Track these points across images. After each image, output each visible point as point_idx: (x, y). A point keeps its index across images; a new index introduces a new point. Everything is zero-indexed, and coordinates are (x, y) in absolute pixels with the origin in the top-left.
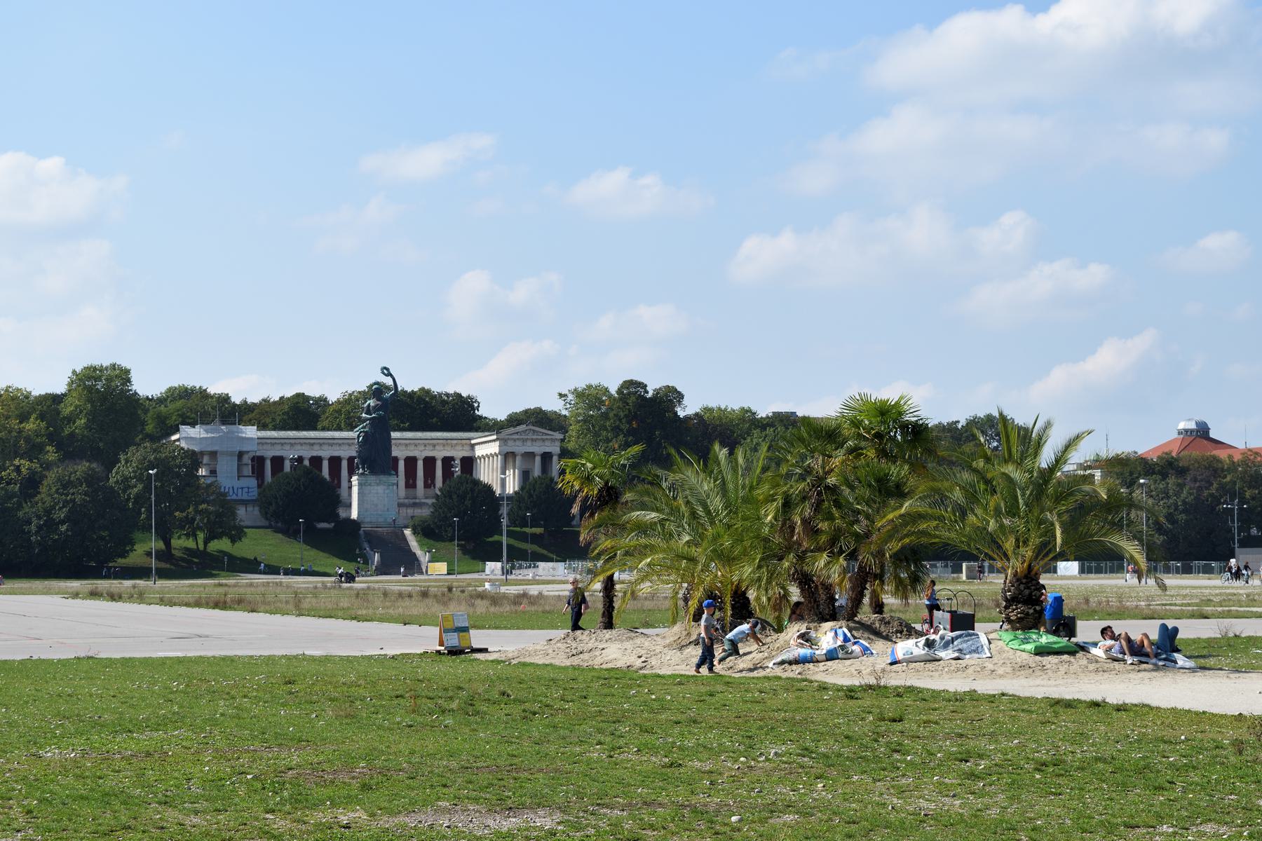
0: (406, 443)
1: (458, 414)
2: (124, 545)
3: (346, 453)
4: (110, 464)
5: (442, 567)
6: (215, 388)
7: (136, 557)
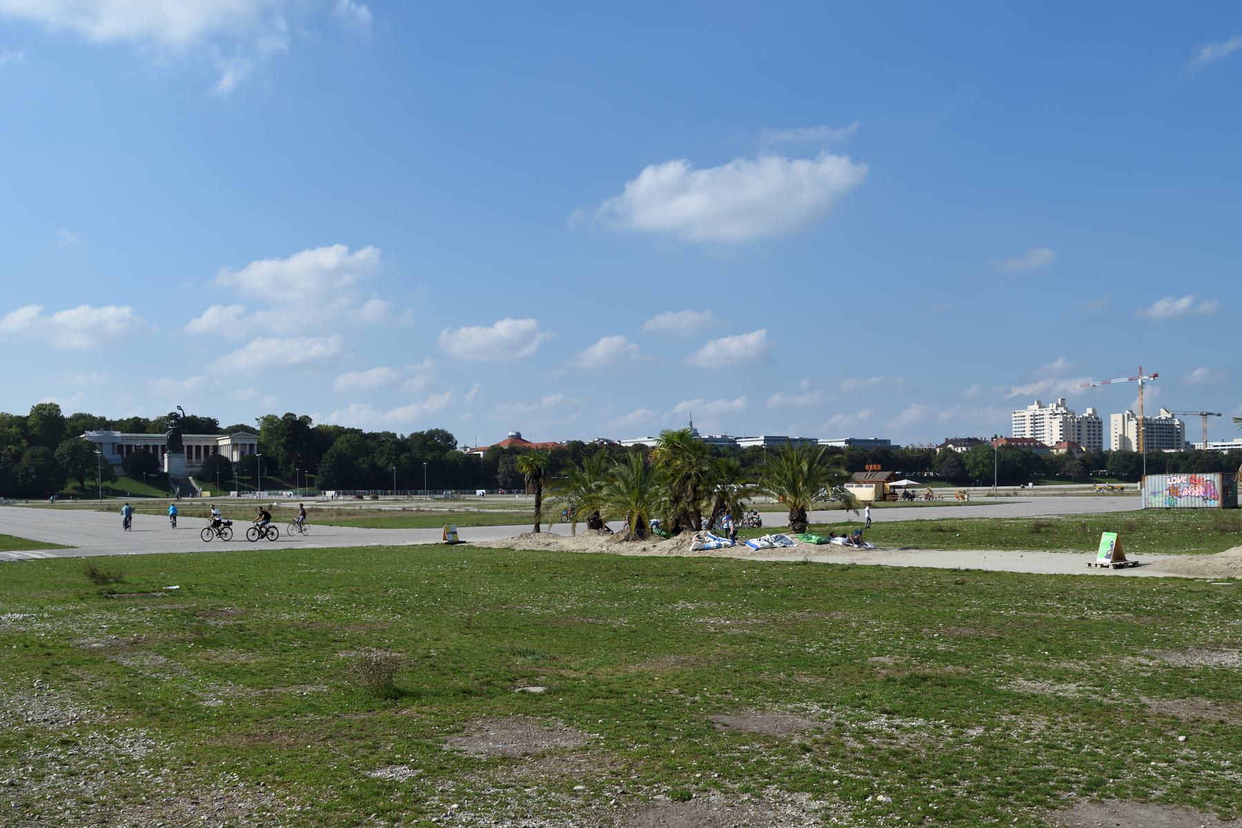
0: (188, 439)
1: (209, 426)
2: (62, 484)
3: (160, 443)
4: (54, 448)
5: (208, 494)
6: (96, 414)
7: (68, 489)
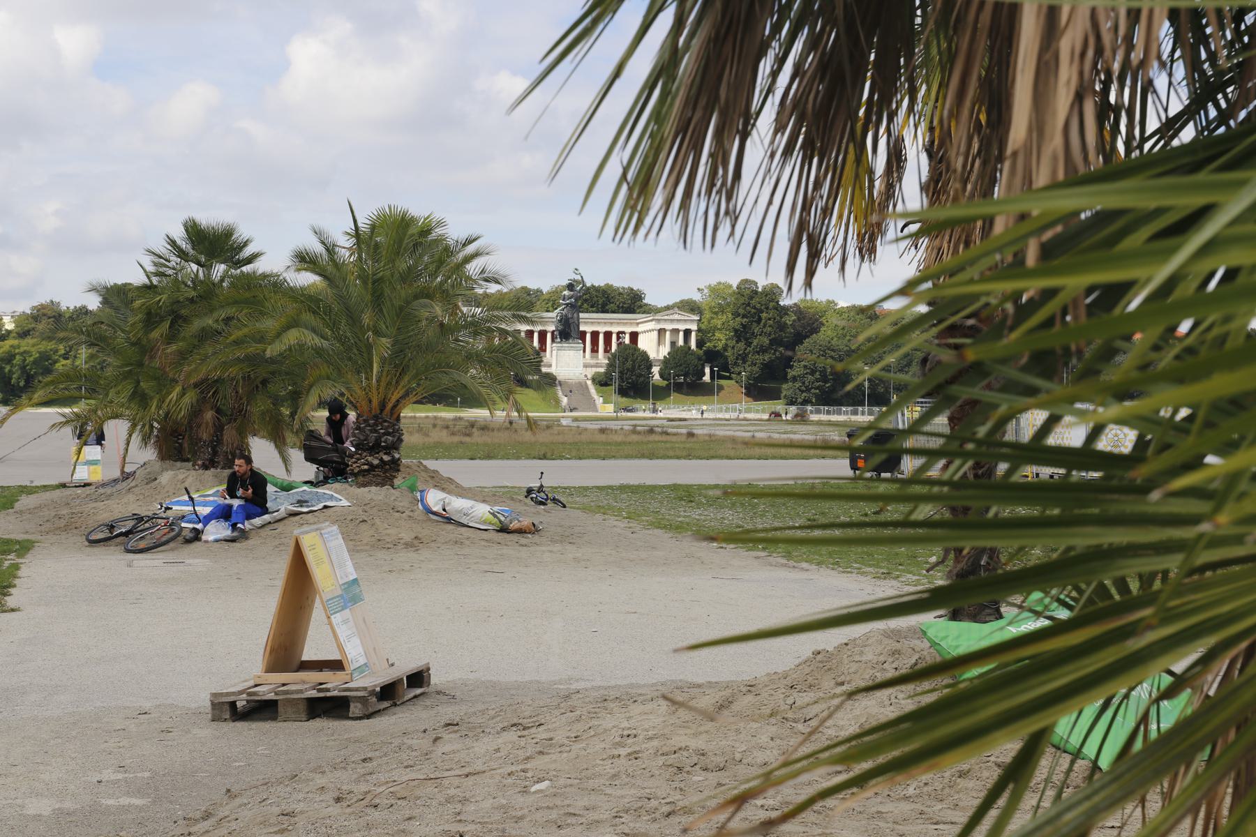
0: (590, 323)
1: (631, 303)
5: (610, 408)
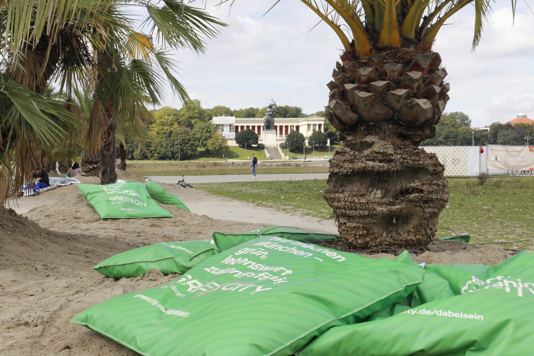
0: (279, 122)
1: (296, 113)
